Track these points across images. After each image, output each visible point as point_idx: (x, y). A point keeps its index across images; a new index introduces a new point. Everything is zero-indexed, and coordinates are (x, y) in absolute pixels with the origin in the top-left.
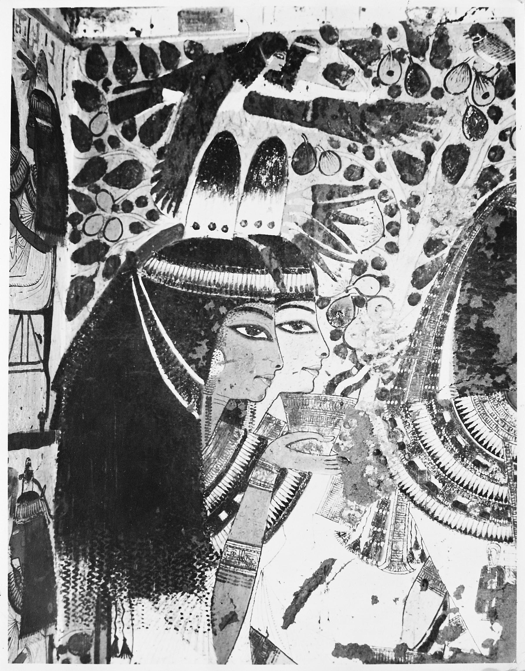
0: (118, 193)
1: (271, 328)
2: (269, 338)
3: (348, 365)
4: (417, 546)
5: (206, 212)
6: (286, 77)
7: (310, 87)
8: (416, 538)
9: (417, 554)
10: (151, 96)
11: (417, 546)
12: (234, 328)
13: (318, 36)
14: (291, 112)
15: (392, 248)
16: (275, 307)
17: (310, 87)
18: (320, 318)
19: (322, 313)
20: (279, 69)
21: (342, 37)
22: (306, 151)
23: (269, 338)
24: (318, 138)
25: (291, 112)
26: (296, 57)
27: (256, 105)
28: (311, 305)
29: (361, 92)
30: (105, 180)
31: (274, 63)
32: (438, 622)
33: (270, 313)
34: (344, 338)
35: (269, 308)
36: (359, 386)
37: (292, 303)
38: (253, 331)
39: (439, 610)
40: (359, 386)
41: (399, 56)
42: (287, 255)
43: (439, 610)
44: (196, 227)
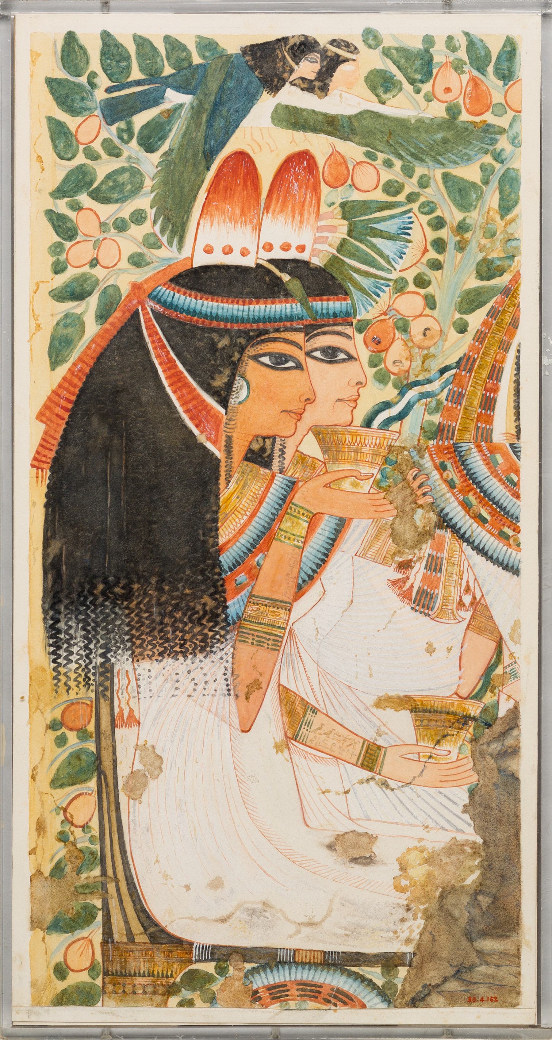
0: (106, 211)
1: (300, 355)
2: (299, 367)
3: (390, 393)
4: (468, 589)
5: (219, 239)
6: (320, 84)
7: (347, 97)
8: (468, 582)
9: (467, 599)
10: (150, 100)
11: (468, 589)
12: (256, 358)
13: (358, 42)
14: (332, 125)
15: (436, 266)
16: (305, 336)
17: (347, 97)
18: (358, 345)
19: (359, 338)
20: (312, 76)
21: (387, 43)
22: (338, 160)
23: (299, 367)
24: (352, 151)
25: (332, 125)
26: (331, 64)
27: (293, 119)
28: (348, 330)
29: (404, 105)
30: (91, 195)
31: (308, 68)
32: (489, 669)
33: (302, 344)
34: (385, 363)
35: (299, 337)
36: (401, 416)
37: (326, 329)
38: (279, 361)
39: (492, 658)
40: (401, 416)
41: (458, 67)
42: (322, 281)
43: (492, 658)
44: (209, 250)
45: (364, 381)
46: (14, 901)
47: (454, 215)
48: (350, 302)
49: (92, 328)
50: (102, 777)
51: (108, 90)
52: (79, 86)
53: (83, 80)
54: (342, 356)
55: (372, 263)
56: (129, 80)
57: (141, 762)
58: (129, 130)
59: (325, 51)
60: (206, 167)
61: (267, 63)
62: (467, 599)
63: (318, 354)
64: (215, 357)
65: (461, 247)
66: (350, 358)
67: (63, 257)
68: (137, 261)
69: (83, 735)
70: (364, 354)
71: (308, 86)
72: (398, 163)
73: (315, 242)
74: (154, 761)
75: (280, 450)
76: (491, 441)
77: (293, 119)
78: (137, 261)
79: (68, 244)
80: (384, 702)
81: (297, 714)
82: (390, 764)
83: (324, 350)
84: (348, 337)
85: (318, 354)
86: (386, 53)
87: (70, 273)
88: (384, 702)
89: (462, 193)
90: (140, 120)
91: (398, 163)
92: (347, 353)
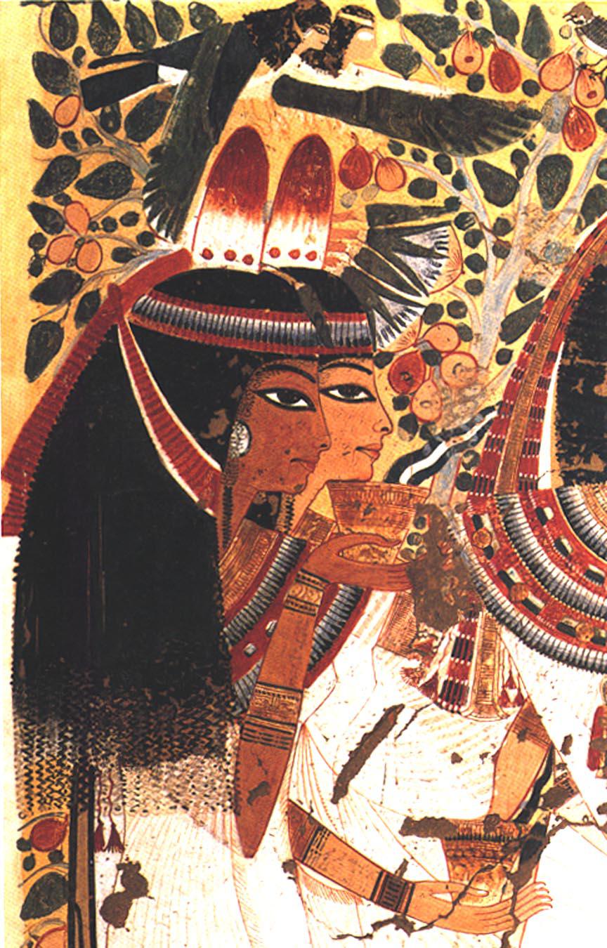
6: (330, 59)
8: (510, 672)
17: (361, 74)
18: (380, 381)
27: (288, 92)
28: (368, 364)
29: (429, 84)
45: (389, 426)
46: (12, 598)
47: (490, 214)
48: (365, 322)
49: (72, 333)
50: (76, 914)
51: (94, 65)
52: (62, 62)
53: (68, 55)
54: (362, 395)
55: (401, 285)
56: (116, 52)
57: (122, 883)
58: (116, 115)
59: (339, 20)
60: (199, 155)
61: (265, 36)
62: (512, 694)
63: (336, 393)
64: (210, 382)
65: (502, 251)
66: (371, 399)
67: (43, 252)
68: (122, 255)
69: (56, 857)
70: (387, 396)
71: (314, 58)
72: (431, 154)
73: (327, 250)
74: (134, 882)
75: (287, 507)
76: (537, 488)
77: (288, 92)
78: (122, 255)
79: (50, 238)
80: (411, 827)
81: (309, 838)
82: (419, 906)
83: (340, 388)
84: (369, 372)
85: (336, 393)
86: (409, 22)
87: (48, 271)
88: (411, 827)
89: (499, 188)
90: (127, 104)
91: (431, 154)
92: (367, 392)
